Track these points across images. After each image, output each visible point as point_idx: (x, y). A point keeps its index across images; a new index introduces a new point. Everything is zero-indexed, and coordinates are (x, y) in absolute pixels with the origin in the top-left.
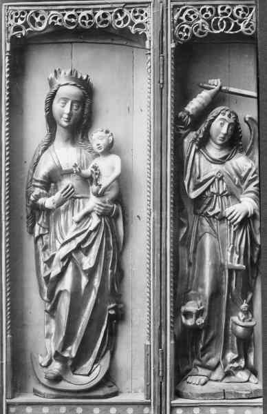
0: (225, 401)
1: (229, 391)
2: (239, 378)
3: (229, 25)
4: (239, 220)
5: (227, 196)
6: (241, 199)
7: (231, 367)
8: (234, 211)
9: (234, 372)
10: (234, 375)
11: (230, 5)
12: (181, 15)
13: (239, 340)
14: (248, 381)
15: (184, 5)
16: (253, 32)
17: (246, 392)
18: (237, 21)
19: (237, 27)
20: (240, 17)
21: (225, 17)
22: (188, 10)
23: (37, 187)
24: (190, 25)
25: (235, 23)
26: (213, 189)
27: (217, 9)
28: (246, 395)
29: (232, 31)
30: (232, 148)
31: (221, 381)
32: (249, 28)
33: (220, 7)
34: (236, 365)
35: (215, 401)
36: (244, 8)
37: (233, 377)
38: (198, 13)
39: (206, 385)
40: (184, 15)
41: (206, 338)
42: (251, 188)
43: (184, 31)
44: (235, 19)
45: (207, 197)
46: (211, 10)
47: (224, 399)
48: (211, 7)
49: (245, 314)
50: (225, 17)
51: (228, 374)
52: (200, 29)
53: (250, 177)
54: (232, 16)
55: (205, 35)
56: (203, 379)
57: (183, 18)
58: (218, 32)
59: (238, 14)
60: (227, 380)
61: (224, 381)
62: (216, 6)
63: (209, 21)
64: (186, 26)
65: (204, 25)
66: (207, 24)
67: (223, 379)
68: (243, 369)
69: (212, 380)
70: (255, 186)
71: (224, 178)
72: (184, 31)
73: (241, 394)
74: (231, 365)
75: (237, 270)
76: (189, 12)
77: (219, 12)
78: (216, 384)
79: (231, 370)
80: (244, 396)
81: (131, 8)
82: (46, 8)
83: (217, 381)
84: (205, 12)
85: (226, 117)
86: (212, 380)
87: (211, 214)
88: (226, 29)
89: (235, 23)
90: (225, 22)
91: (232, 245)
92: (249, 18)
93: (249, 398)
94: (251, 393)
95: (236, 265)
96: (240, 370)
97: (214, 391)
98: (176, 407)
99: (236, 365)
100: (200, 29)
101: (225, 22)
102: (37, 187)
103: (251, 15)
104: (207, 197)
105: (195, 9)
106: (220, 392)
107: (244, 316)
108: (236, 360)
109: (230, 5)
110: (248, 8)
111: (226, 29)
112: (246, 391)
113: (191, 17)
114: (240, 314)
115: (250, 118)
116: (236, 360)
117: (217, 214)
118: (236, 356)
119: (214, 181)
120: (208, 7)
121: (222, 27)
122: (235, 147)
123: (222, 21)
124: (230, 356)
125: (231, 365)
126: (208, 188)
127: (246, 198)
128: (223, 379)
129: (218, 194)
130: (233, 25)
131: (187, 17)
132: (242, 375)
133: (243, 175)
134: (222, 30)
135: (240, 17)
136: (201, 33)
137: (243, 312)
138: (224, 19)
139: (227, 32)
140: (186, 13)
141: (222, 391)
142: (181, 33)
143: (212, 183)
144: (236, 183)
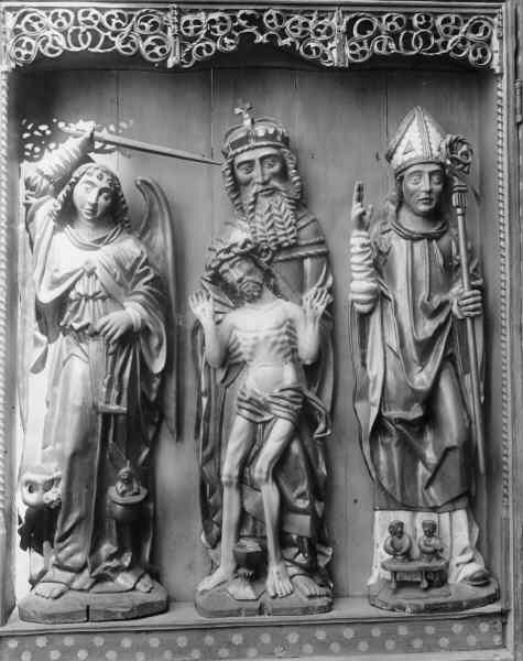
0: (88, 624)
1: (96, 608)
2: (119, 585)
3: (96, 37)
4: (115, 337)
5: (103, 299)
6: (125, 304)
7: (105, 569)
8: (107, 323)
9: (112, 575)
10: (112, 580)
11: (96, 8)
12: (19, 22)
13: (120, 525)
14: (134, 589)
15: (23, 7)
16: (134, 50)
17: (124, 610)
18: (109, 34)
19: (108, 43)
20: (113, 28)
21: (90, 27)
22: (30, 15)
23: (244, 408)
24: (34, 38)
25: (106, 37)
26: (80, 288)
27: (76, 14)
28: (123, 613)
29: (101, 48)
30: (116, 224)
31: (88, 590)
32: (129, 46)
33: (81, 11)
34: (115, 563)
35: (72, 626)
36: (119, 14)
37: (110, 584)
38: (47, 20)
39: (62, 598)
40: (23, 22)
41: (62, 526)
42: (141, 287)
43: (24, 45)
44: (106, 30)
45: (71, 301)
46: (65, 15)
47: (87, 621)
48: (401, 16)
49: (127, 484)
50: (90, 27)
51: (100, 579)
52: (49, 45)
53: (138, 271)
54: (100, 26)
55: (58, 54)
56: (57, 588)
57: (21, 26)
58: (78, 49)
59: (110, 23)
60: (97, 588)
61: (92, 590)
62: (75, 10)
63: (65, 33)
64: (27, 40)
65: (56, 38)
66: (61, 36)
67: (91, 587)
68: (128, 569)
69: (73, 589)
70: (146, 284)
71: (97, 272)
72: (24, 45)
73: (115, 613)
74: (108, 564)
75: (116, 415)
76: (31, 18)
77: (80, 19)
78: (79, 594)
79: (108, 572)
80: (119, 616)
81: (53, 8)
82: (373, 9)
83: (81, 590)
84: (57, 18)
85: (94, 179)
86: (73, 589)
87: (77, 326)
88: (92, 45)
89: (106, 37)
90: (421, 40)
91: (109, 376)
92: (127, 29)
93: (127, 619)
94: (132, 610)
95: (114, 407)
96: (123, 571)
97: (69, 609)
98: (7, 636)
99: (115, 563)
100: (49, 45)
101: (421, 40)
102: (244, 408)
103: (130, 25)
104: (71, 301)
105: (43, 13)
106: (80, 611)
107: (124, 488)
108: (117, 555)
109: (96, 8)
110: (126, 14)
111: (92, 45)
112: (122, 607)
113: (35, 25)
114: (119, 484)
115: (142, 181)
116: (117, 555)
117: (87, 326)
118: (115, 549)
119: (82, 274)
120: (60, 11)
121: (85, 42)
122: (119, 226)
123: (84, 33)
124: (107, 548)
125: (108, 564)
126: (72, 287)
127: (130, 304)
128: (91, 587)
129: (87, 298)
130: (102, 40)
131: (27, 24)
132: (124, 580)
133: (128, 267)
134: (84, 47)
135: (113, 28)
136: (52, 51)
137: (123, 480)
138: (89, 30)
139: (93, 50)
140: (27, 19)
141: (85, 608)
142: (19, 49)
143: (78, 279)
144: (118, 278)
